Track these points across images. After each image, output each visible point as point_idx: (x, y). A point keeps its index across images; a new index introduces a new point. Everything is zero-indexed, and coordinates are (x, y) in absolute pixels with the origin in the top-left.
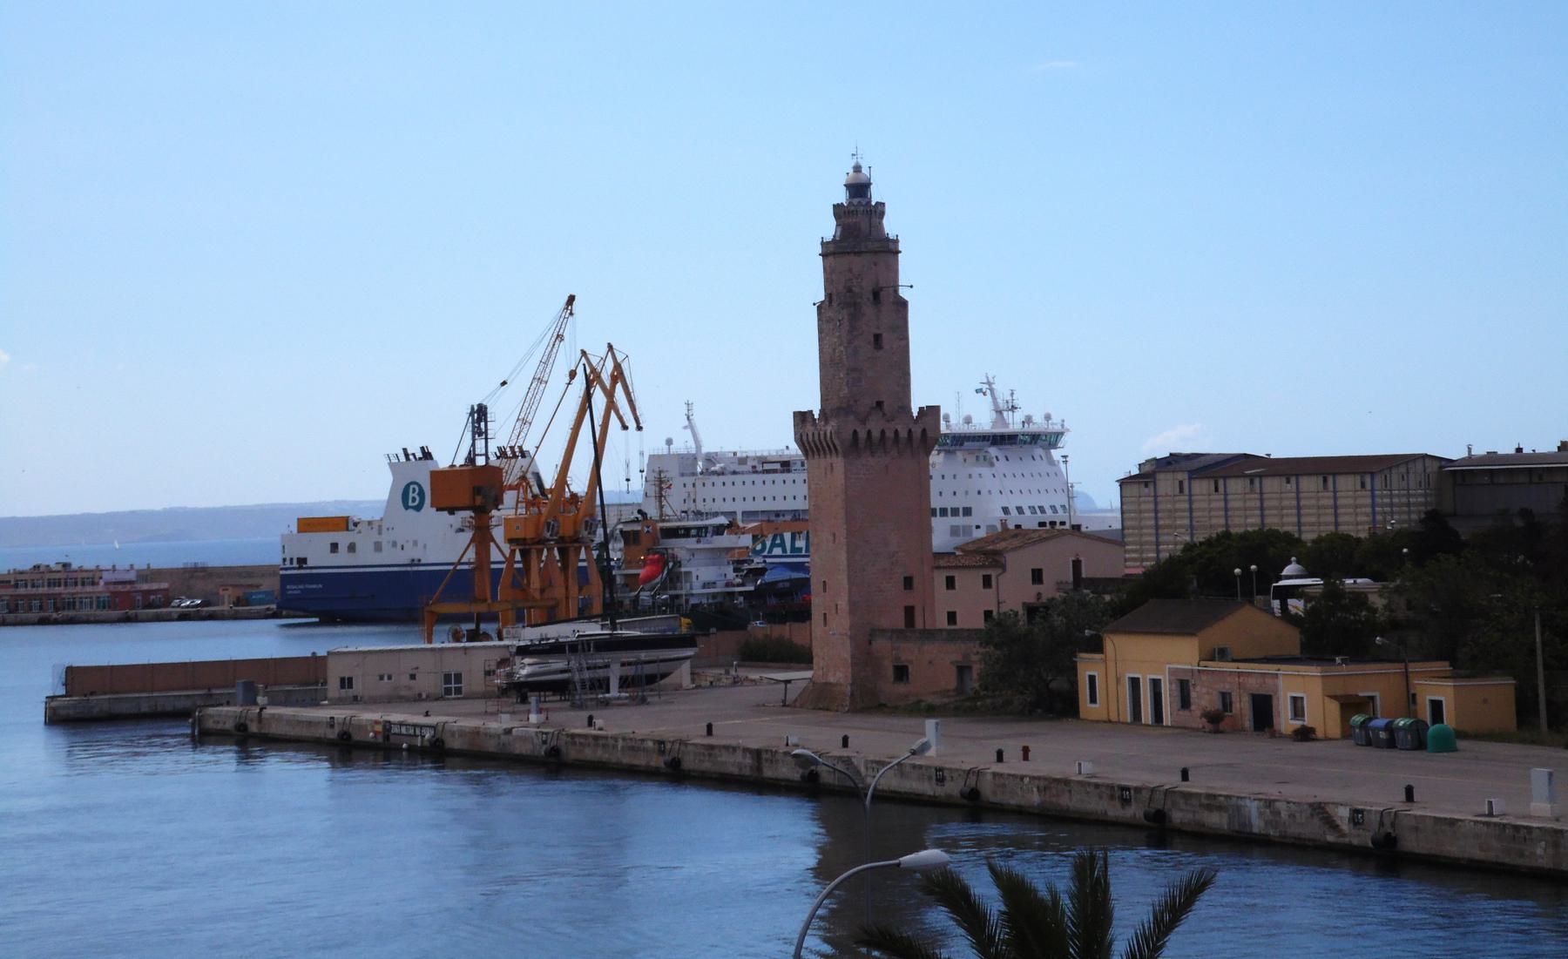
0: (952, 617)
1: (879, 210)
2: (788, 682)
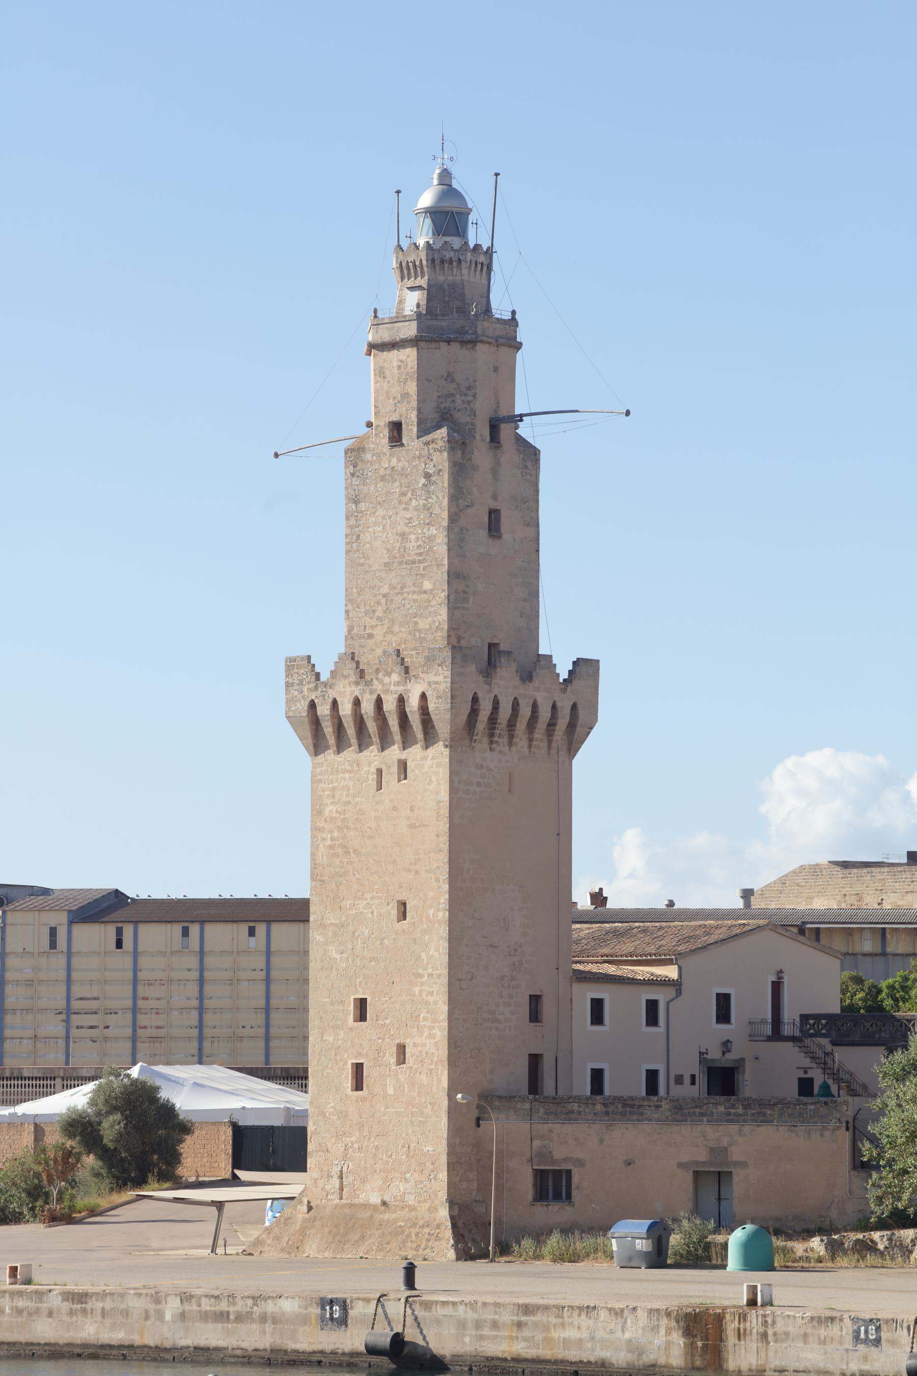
1: (484, 260)
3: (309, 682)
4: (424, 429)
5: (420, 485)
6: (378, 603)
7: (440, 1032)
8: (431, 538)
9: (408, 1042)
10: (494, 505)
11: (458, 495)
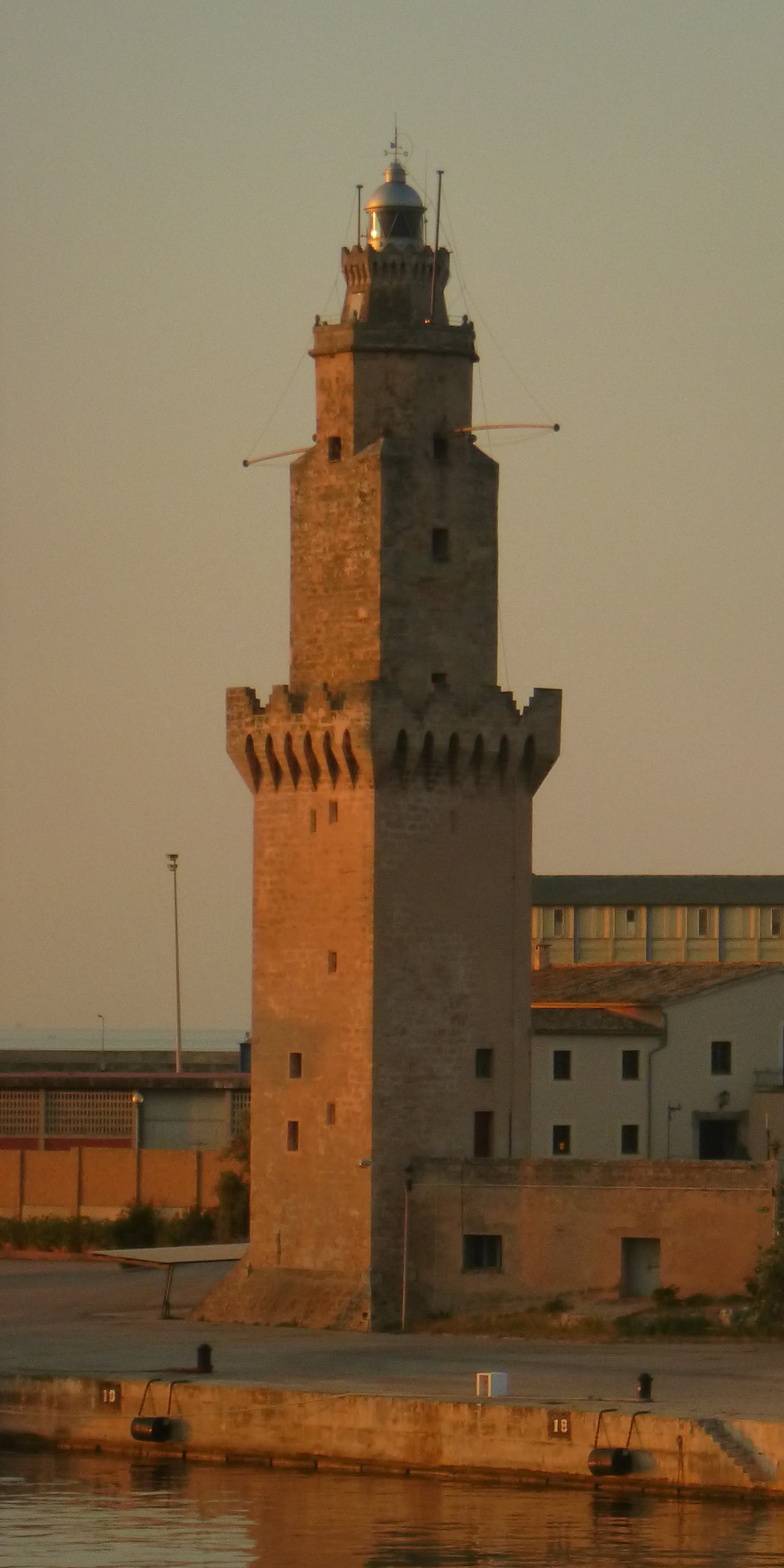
0: (562, 1134)
1: (437, 265)
2: (172, 1265)
3: (246, 716)
5: (356, 505)
6: (318, 631)
7: (365, 1092)
8: (365, 563)
10: (441, 524)
11: (393, 518)
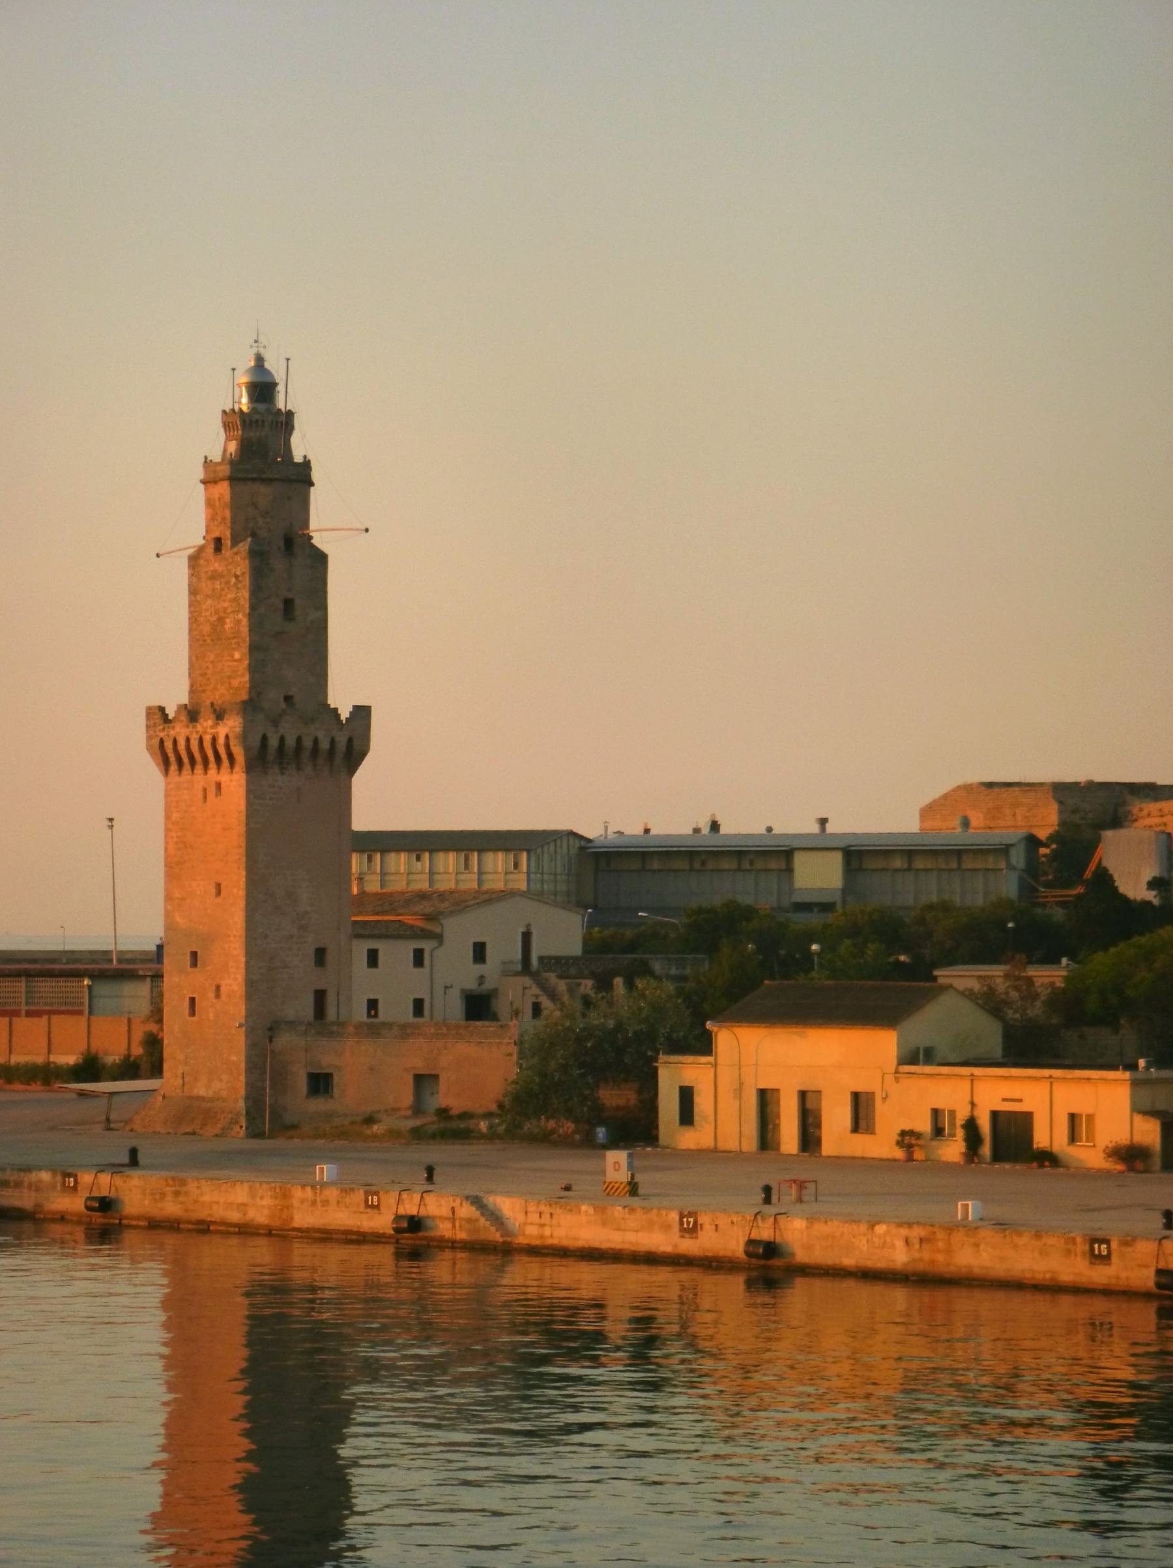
0: (373, 1005)
1: (286, 422)
2: (112, 1094)
4: (235, 541)
7: (240, 977)
9: (223, 983)
10: (290, 595)
11: (256, 591)
